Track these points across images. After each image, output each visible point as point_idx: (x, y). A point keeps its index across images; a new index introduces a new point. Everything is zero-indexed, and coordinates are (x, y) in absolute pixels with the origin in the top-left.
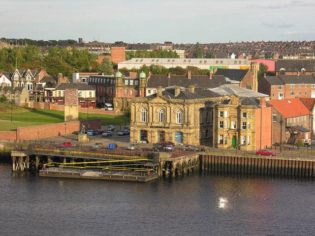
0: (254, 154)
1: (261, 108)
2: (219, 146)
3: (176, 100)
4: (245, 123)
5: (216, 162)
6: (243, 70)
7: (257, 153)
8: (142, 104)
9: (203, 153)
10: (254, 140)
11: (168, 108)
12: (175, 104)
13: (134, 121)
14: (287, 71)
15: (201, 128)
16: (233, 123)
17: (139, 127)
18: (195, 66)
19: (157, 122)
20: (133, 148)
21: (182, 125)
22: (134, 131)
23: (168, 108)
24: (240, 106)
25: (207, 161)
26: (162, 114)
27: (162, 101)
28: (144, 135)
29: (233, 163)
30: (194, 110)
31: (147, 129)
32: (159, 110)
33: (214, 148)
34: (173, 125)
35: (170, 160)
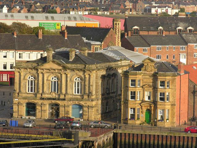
0: (182, 132)
1: (180, 75)
2: (130, 122)
3: (73, 66)
4: (163, 94)
5: (135, 141)
6: (103, 29)
7: (186, 131)
8: (29, 70)
9: (119, 131)
10: (174, 115)
11: (64, 76)
12: (73, 70)
13: (18, 91)
14: (142, 30)
15: (102, 100)
16: (147, 94)
17: (25, 98)
18: (23, 22)
19: (48, 92)
20: (31, 125)
21: (82, 96)
22: (19, 104)
23: (64, 76)
24: (157, 73)
25: (123, 140)
26: (55, 82)
27: (55, 66)
28: (31, 108)
29: (156, 142)
30: (95, 78)
31: (36, 101)
32: (52, 78)
33: (122, 124)
34: (70, 96)
35: (91, 139)
